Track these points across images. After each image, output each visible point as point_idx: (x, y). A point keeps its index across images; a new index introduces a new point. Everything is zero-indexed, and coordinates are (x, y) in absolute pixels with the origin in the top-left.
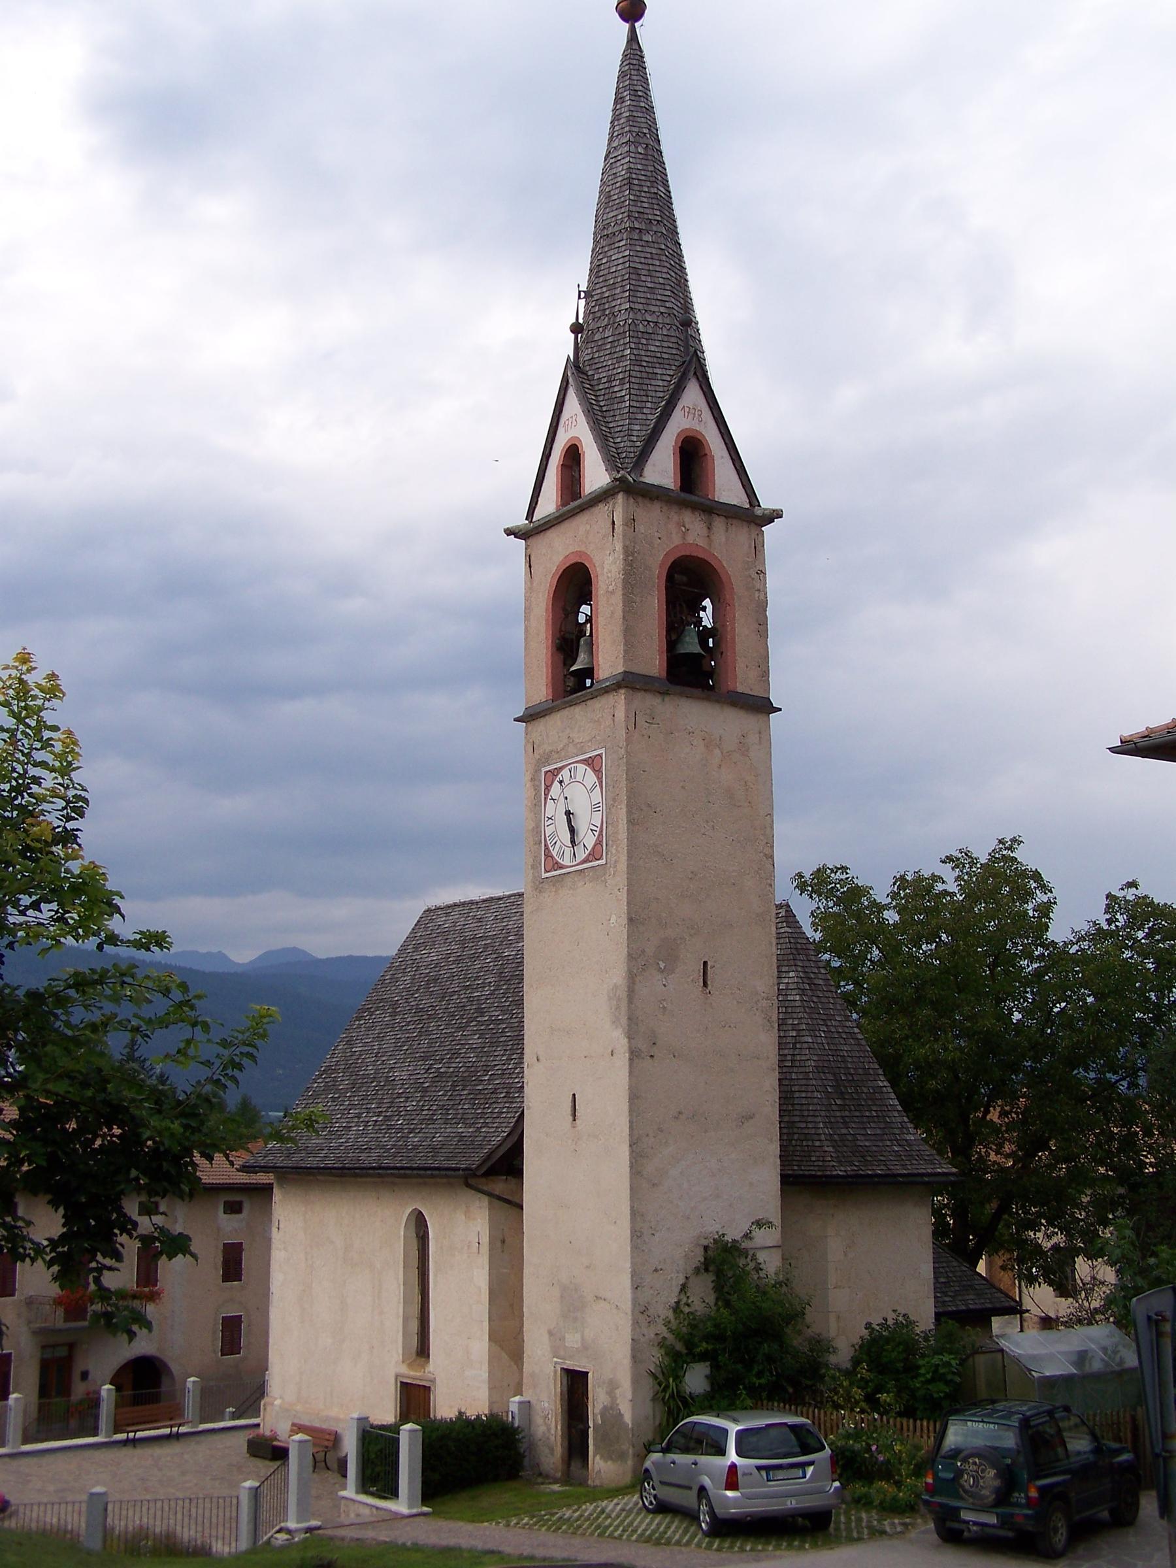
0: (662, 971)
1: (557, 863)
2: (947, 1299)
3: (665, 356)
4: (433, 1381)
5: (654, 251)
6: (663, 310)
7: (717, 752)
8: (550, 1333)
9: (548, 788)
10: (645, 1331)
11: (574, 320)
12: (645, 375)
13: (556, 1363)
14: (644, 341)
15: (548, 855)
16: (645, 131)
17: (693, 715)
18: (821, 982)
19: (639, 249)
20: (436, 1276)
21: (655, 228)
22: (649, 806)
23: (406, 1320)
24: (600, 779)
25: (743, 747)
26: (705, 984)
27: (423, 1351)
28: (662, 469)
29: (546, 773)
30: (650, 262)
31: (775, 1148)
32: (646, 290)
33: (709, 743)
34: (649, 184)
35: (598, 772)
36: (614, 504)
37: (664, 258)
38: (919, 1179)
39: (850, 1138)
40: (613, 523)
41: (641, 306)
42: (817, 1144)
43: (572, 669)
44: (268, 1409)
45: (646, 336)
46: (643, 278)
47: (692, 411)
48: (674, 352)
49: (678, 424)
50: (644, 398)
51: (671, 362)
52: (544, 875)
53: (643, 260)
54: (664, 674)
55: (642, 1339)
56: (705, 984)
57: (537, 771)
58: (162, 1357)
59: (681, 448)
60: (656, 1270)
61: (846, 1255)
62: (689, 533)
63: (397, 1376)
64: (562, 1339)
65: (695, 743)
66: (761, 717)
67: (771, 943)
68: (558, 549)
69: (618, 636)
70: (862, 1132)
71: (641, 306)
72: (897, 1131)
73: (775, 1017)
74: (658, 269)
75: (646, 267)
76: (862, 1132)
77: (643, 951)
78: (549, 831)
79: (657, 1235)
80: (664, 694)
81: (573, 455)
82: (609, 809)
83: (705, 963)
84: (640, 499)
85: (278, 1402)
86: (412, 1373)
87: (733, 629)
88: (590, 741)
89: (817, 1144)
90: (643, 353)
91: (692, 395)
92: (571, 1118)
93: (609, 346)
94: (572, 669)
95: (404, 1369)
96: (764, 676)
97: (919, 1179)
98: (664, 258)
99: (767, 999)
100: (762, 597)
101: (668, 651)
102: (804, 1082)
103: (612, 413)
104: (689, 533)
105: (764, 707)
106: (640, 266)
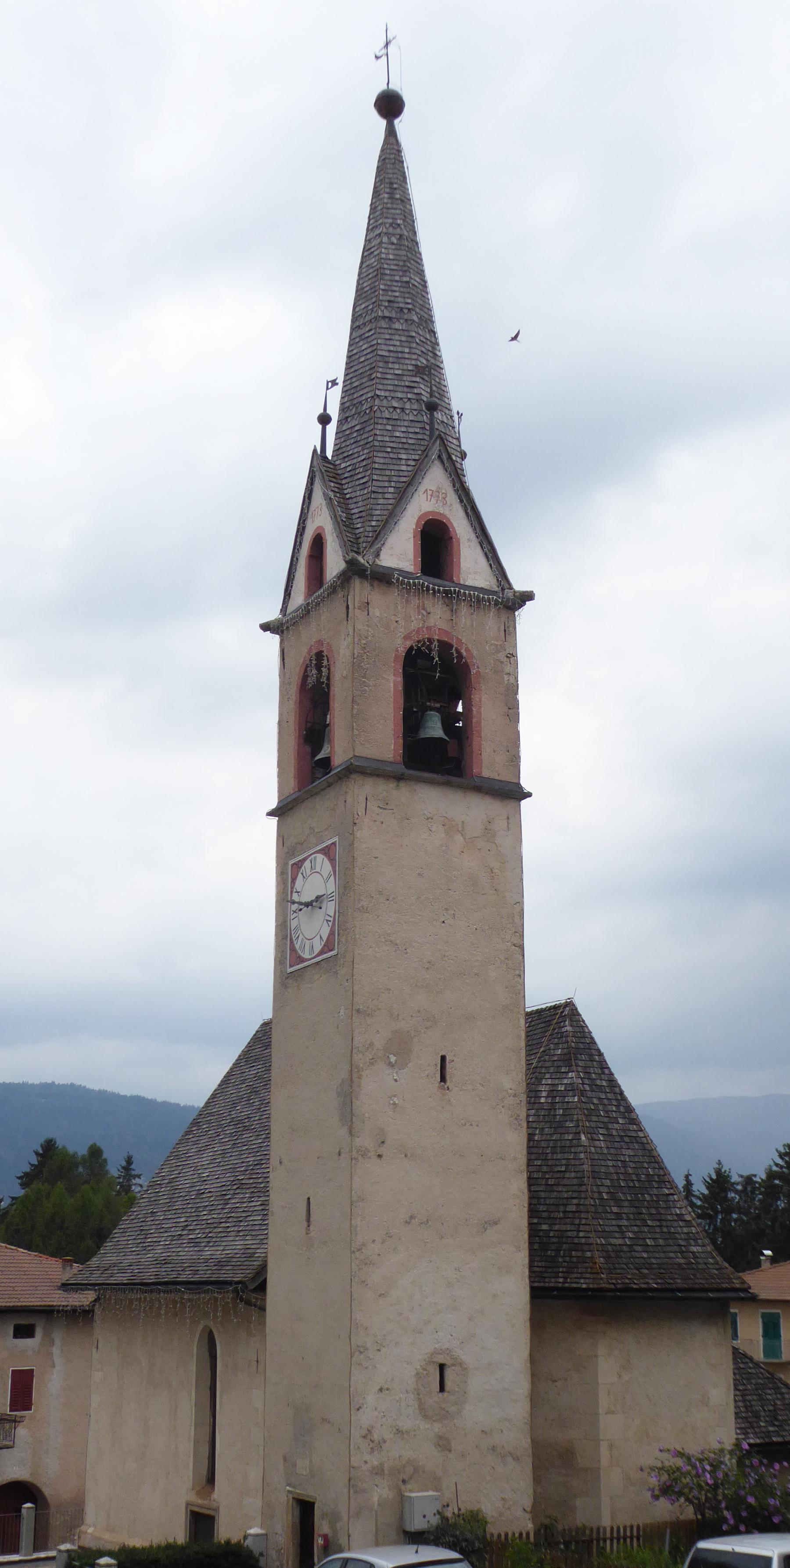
0: (391, 1065)
1: (300, 957)
2: (771, 1429)
3: (410, 441)
4: (217, 1510)
5: (403, 339)
6: (409, 396)
7: (459, 838)
8: (285, 1459)
9: (294, 880)
10: (367, 1457)
11: (322, 411)
12: (390, 461)
13: (289, 1491)
14: (389, 428)
15: (293, 949)
16: (399, 222)
17: (432, 801)
18: (604, 1083)
19: (387, 337)
20: (221, 1398)
21: (406, 317)
22: (380, 893)
23: (196, 1443)
24: (334, 867)
25: (489, 833)
26: (443, 1079)
27: (211, 1479)
28: (400, 551)
29: (293, 865)
30: (400, 349)
31: (523, 1257)
32: (393, 377)
33: (451, 827)
34: (401, 273)
35: (332, 860)
36: (349, 589)
37: (414, 345)
38: (703, 1295)
39: (625, 1248)
40: (348, 607)
41: (387, 394)
42: (588, 1254)
43: (317, 758)
44: (83, 1536)
45: (391, 422)
46: (390, 366)
47: (436, 494)
48: (420, 437)
49: (420, 505)
50: (386, 484)
51: (417, 447)
52: (290, 970)
53: (392, 348)
54: (399, 759)
55: (364, 1468)
56: (443, 1079)
57: (286, 864)
58: (35, 1482)
59: (422, 532)
60: (381, 1390)
61: (620, 1376)
62: (434, 618)
63: (188, 1504)
64: (294, 1465)
65: (434, 829)
66: (512, 803)
67: (519, 1037)
68: (308, 637)
69: (371, 724)
70: (641, 1242)
71: (387, 394)
72: (682, 1243)
73: (523, 1115)
74: (407, 356)
75: (395, 355)
76: (641, 1242)
77: (371, 1045)
78: (294, 924)
79: (383, 1350)
80: (399, 778)
81: (318, 543)
82: (341, 898)
83: (443, 1058)
84: (376, 583)
85: (90, 1530)
86: (200, 1502)
87: (480, 713)
88: (326, 829)
89: (588, 1254)
90: (387, 439)
91: (435, 477)
92: (305, 1224)
93: (355, 435)
94: (317, 758)
95: (193, 1498)
96: (514, 760)
97: (703, 1295)
98: (414, 345)
99: (515, 1096)
100: (512, 680)
101: (405, 736)
102: (576, 1188)
103: (354, 500)
104: (434, 618)
105: (514, 793)
106: (387, 354)
